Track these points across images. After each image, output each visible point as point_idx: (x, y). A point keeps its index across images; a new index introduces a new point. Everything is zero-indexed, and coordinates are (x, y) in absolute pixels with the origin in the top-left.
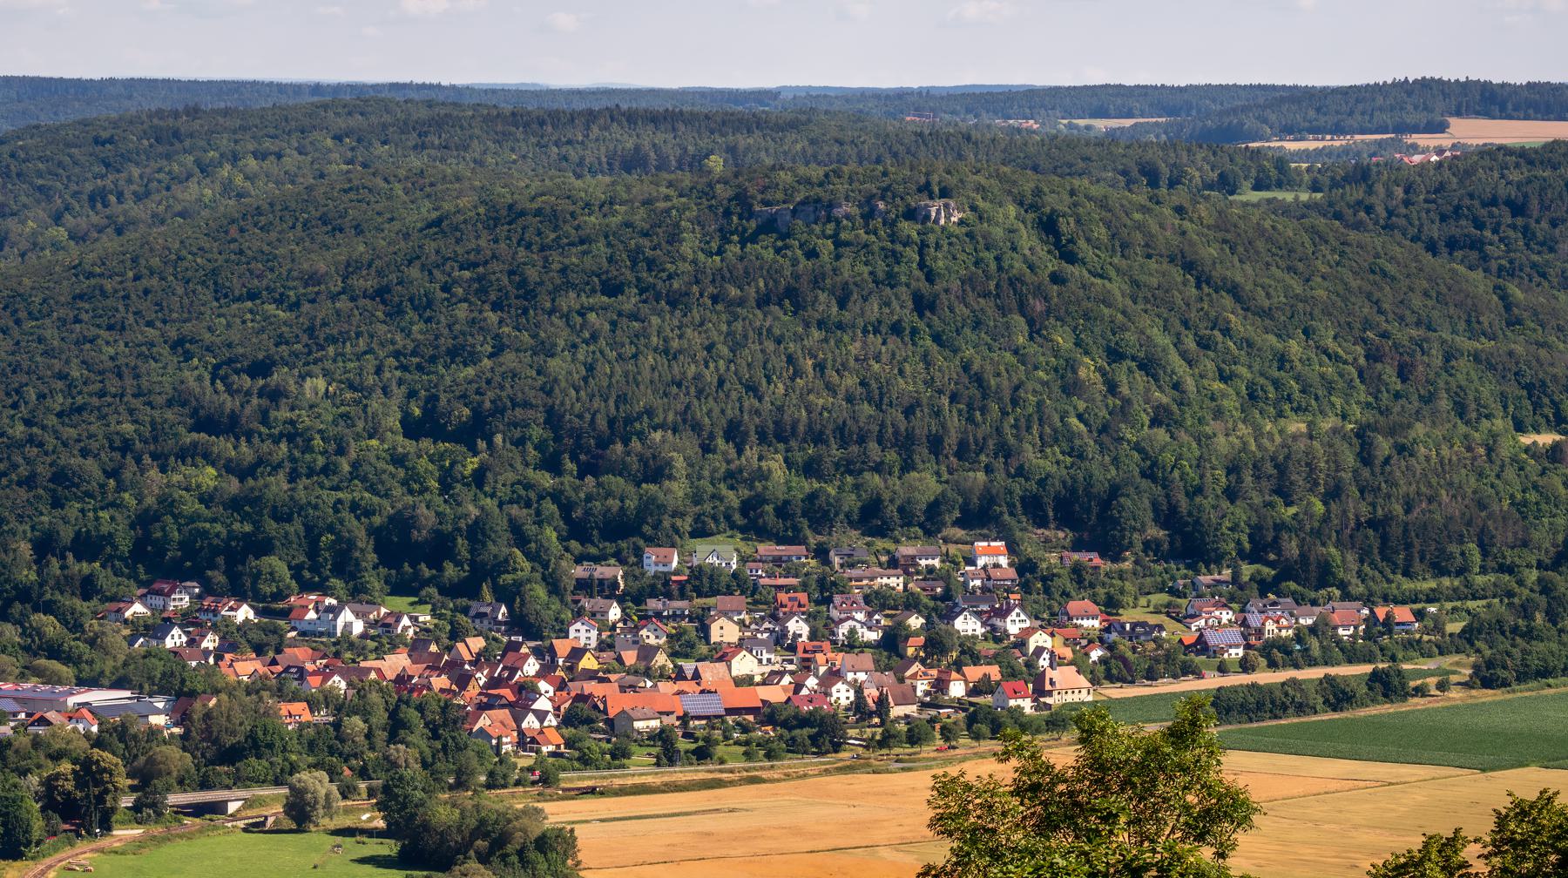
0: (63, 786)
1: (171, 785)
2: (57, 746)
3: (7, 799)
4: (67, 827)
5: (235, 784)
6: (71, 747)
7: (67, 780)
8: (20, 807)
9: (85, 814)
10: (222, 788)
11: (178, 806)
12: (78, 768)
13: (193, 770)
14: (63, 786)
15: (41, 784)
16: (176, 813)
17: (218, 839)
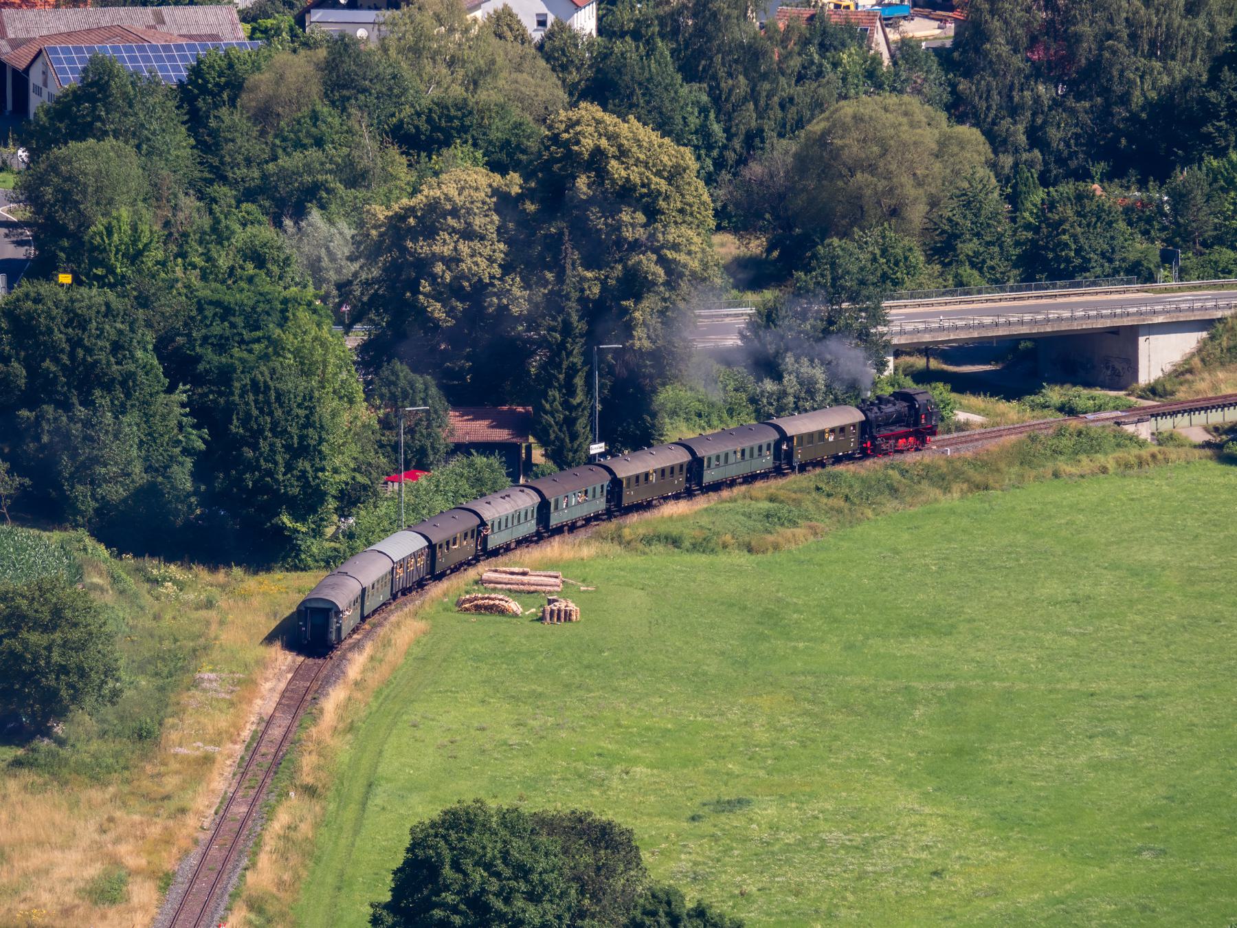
0: (452, 261)
1: (903, 261)
2: (434, 92)
3: (226, 312)
4: (479, 430)
5: (1167, 258)
6: (485, 96)
7: (468, 234)
8: (277, 347)
9: (546, 379)
10: (1111, 276)
11: (926, 350)
12: (514, 183)
13: (994, 199)
14: (452, 261)
15: (367, 250)
16: (924, 377)
17: (1091, 492)
